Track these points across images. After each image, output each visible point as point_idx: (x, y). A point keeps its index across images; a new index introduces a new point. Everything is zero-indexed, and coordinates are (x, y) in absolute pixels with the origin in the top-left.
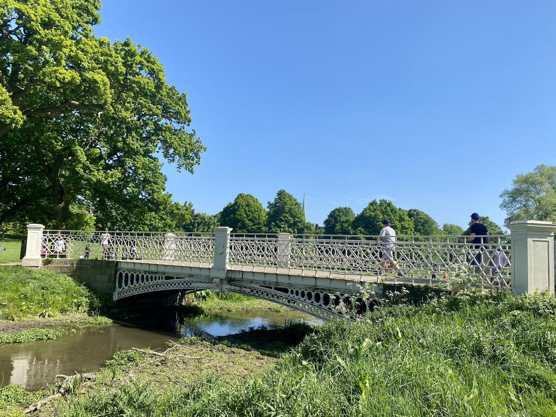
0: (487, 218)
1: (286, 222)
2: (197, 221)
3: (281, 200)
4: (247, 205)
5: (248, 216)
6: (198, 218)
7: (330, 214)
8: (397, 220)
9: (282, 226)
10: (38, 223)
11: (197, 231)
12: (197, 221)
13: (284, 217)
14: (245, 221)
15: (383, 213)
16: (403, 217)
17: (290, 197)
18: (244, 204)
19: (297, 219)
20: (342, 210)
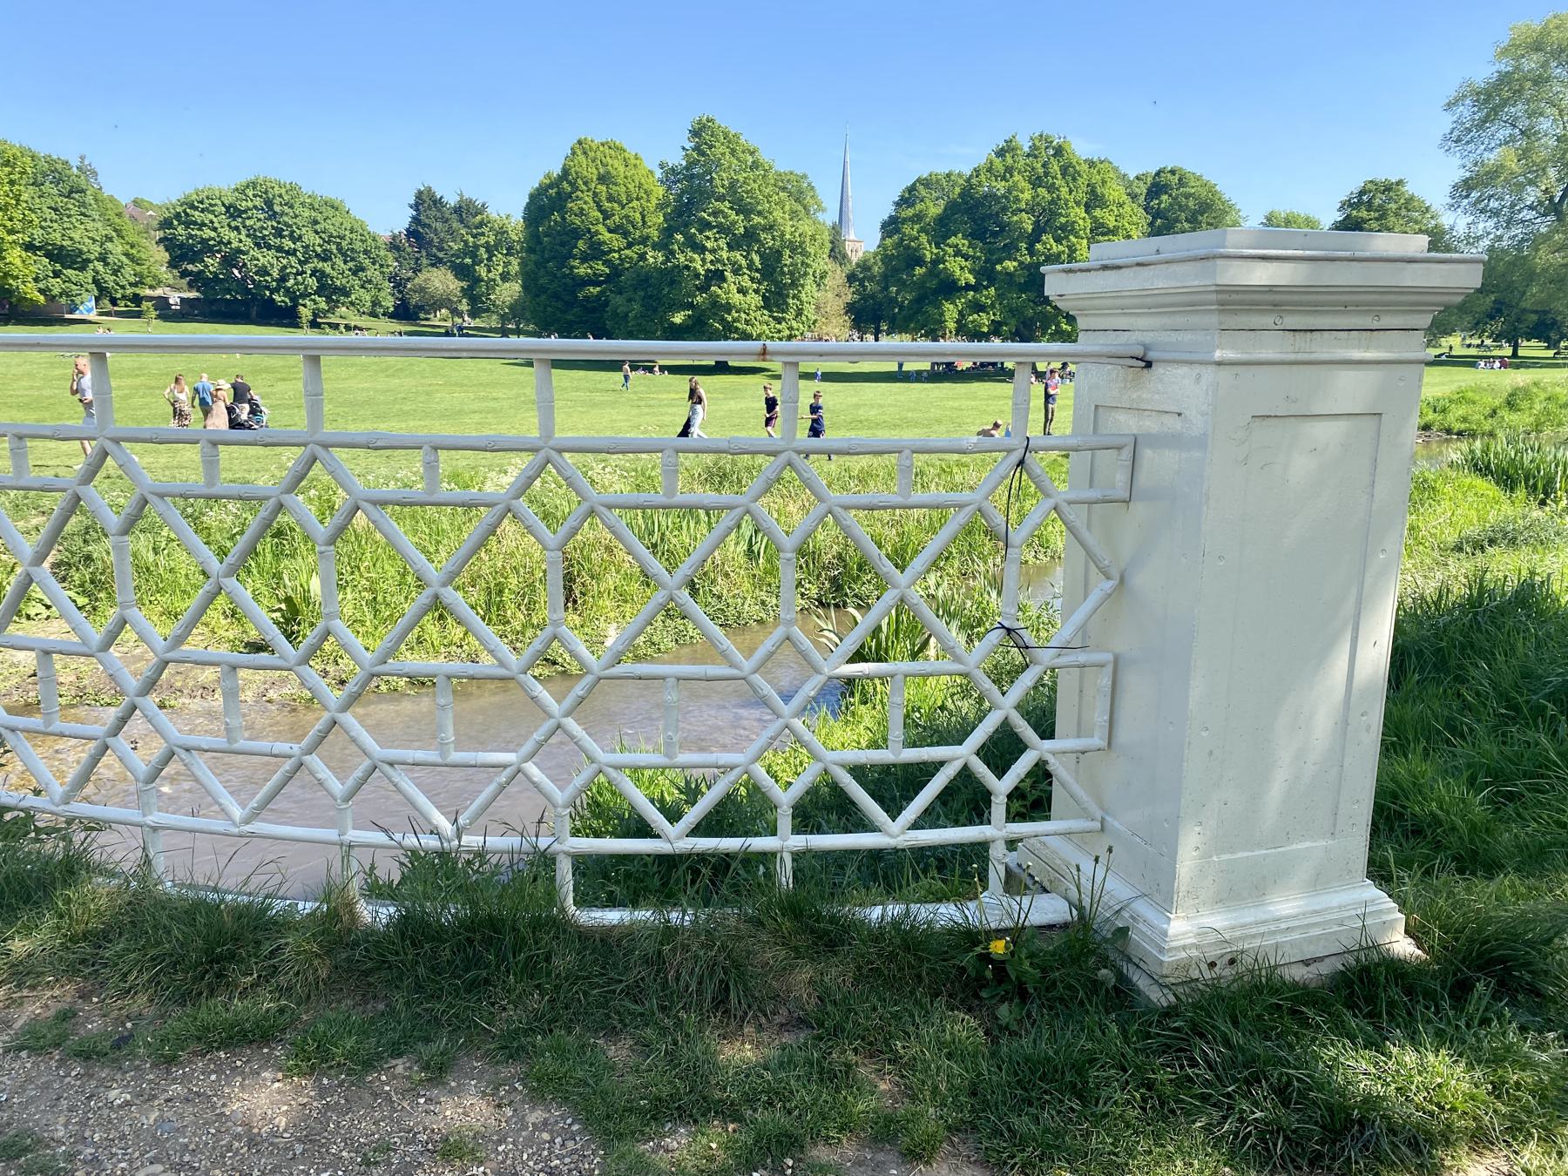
0: (1399, 183)
1: (723, 230)
2: (483, 240)
3: (703, 154)
4: (604, 179)
5: (606, 215)
6: (485, 230)
7: (902, 198)
8: (1078, 203)
9: (709, 245)
10: (658, 339)
11: (489, 271)
12: (483, 240)
13: (715, 214)
14: (597, 233)
15: (1036, 182)
16: (1099, 190)
17: (730, 140)
18: (592, 174)
19: (757, 219)
20: (938, 181)
